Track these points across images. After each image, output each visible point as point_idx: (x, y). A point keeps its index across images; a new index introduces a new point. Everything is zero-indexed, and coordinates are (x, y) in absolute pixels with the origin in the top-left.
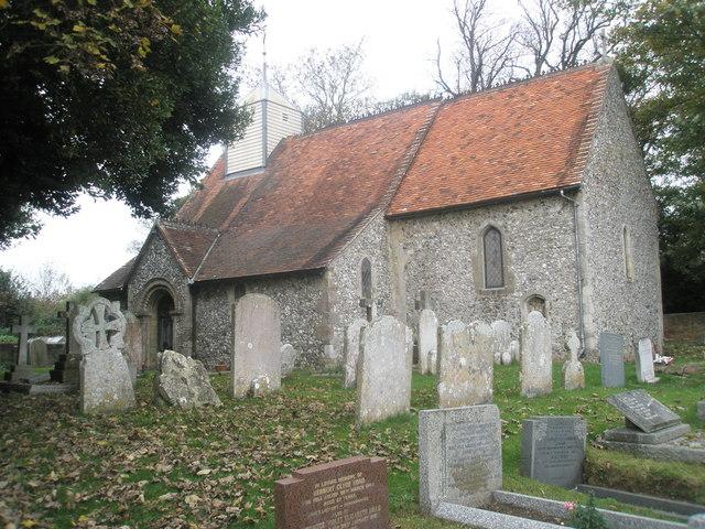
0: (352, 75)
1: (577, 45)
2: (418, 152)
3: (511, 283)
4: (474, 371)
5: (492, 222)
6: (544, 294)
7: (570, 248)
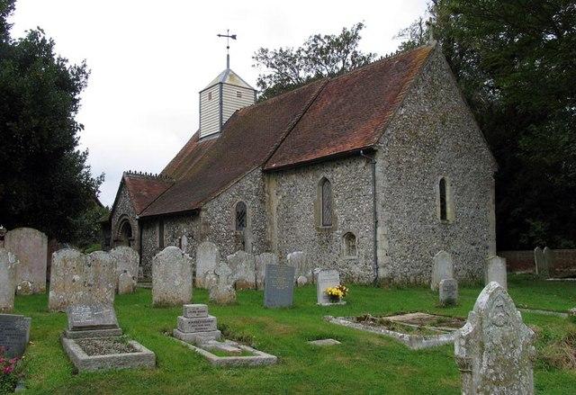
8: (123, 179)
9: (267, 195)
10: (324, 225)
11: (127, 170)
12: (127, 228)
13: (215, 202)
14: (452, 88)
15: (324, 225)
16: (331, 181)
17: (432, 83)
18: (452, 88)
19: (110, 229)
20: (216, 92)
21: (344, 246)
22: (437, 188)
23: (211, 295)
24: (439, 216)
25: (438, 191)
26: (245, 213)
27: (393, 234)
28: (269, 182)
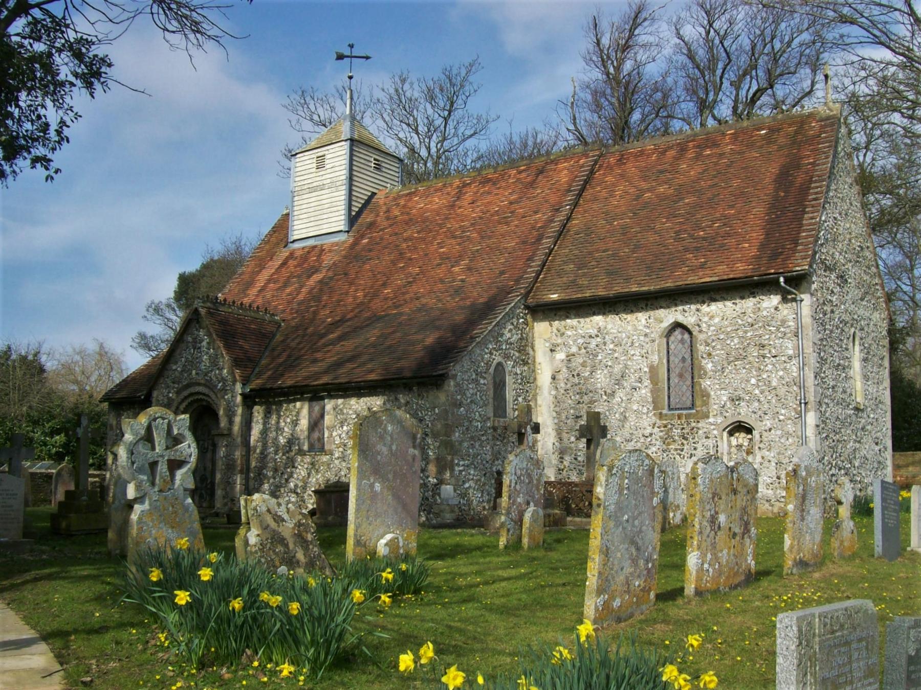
0: (457, 115)
1: (755, 94)
2: (569, 219)
3: (706, 403)
4: (735, 535)
5: (681, 319)
6: (751, 421)
7: (790, 358)
15: (670, 409)
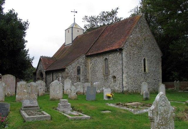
8: (40, 58)
9: (87, 64)
10: (106, 74)
11: (42, 55)
12: (41, 74)
13: (70, 66)
14: (147, 29)
15: (106, 74)
16: (108, 59)
17: (141, 27)
18: (147, 29)
19: (36, 75)
20: (70, 30)
21: (112, 80)
22: (143, 61)
23: (69, 96)
24: (143, 70)
25: (143, 62)
26: (80, 70)
27: (128, 77)
28: (88, 59)
